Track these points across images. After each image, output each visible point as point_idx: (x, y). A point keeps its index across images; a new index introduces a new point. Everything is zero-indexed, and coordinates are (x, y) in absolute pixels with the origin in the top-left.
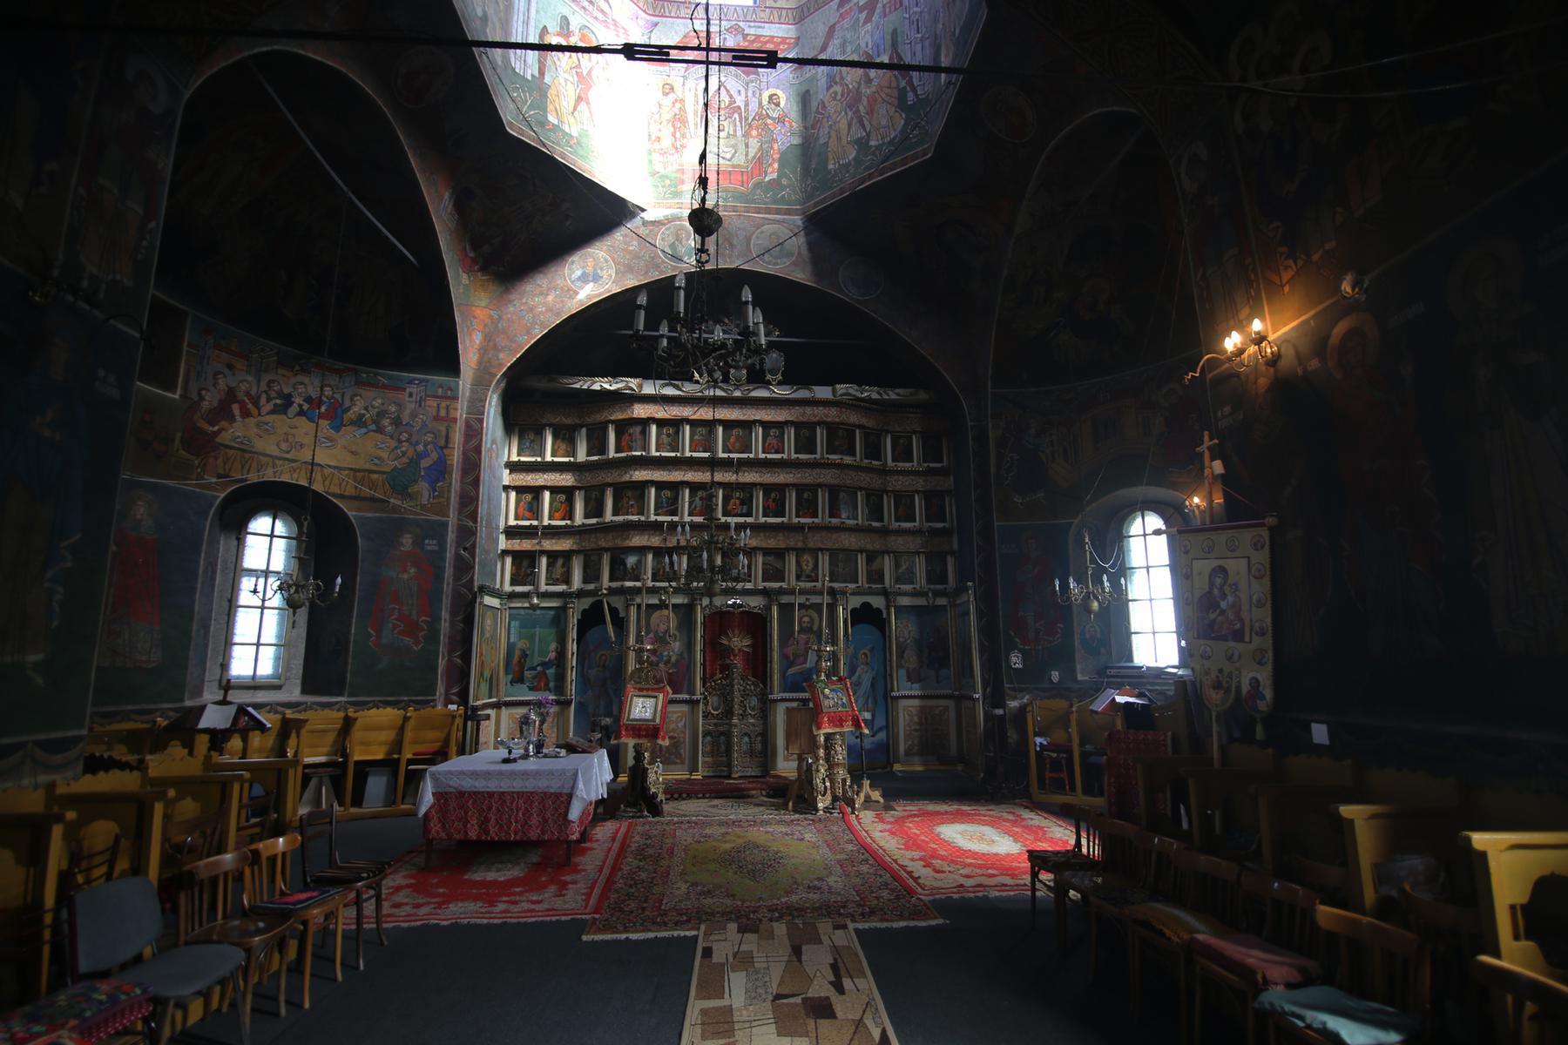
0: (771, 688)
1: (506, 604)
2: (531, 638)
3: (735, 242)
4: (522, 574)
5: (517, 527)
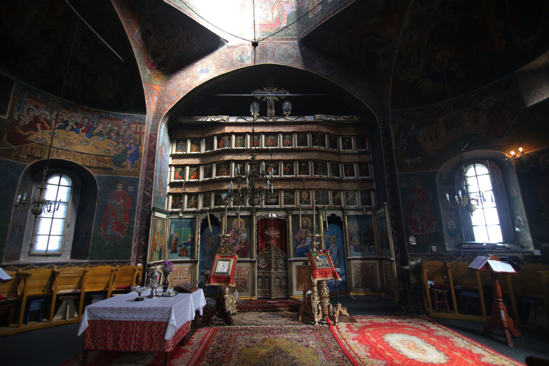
0: (289, 255)
1: (169, 217)
2: (180, 232)
3: (268, 53)
4: (177, 203)
5: (175, 182)
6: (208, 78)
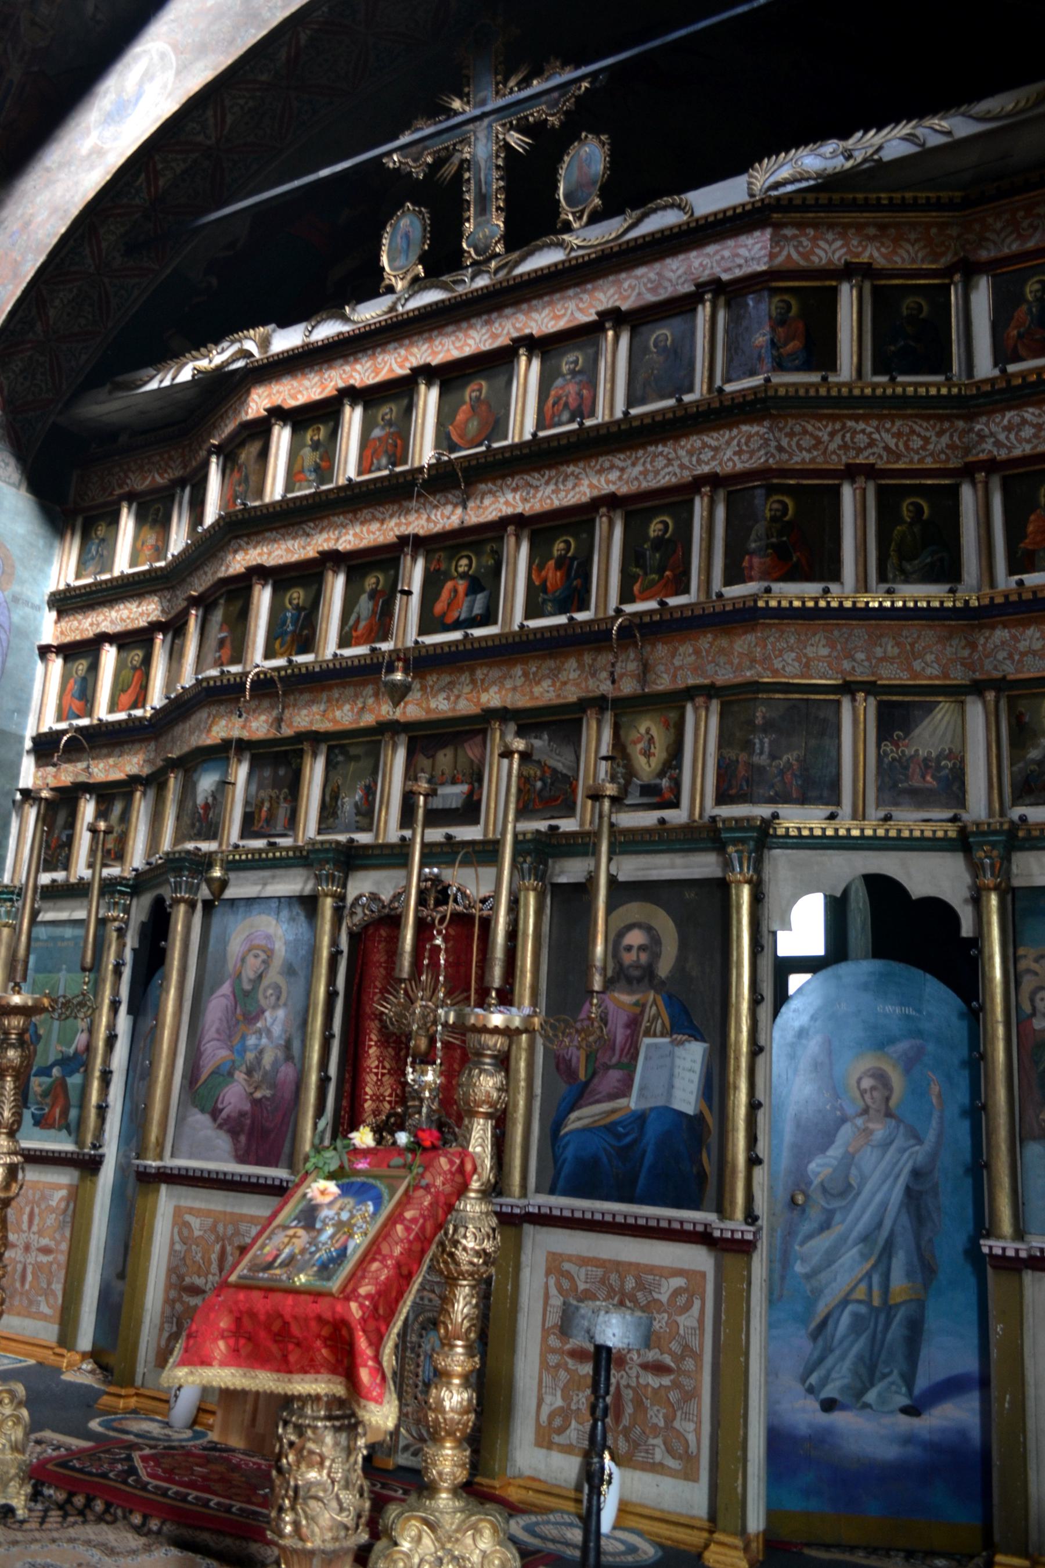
6: (138, 138)
